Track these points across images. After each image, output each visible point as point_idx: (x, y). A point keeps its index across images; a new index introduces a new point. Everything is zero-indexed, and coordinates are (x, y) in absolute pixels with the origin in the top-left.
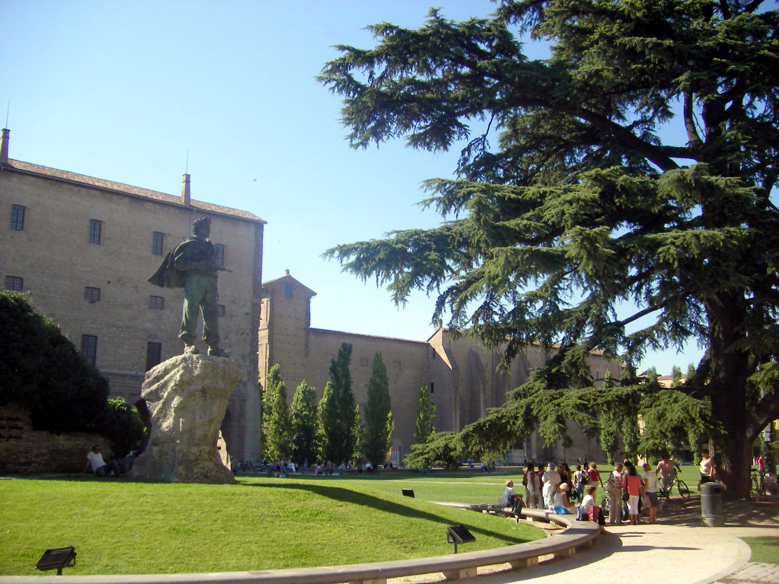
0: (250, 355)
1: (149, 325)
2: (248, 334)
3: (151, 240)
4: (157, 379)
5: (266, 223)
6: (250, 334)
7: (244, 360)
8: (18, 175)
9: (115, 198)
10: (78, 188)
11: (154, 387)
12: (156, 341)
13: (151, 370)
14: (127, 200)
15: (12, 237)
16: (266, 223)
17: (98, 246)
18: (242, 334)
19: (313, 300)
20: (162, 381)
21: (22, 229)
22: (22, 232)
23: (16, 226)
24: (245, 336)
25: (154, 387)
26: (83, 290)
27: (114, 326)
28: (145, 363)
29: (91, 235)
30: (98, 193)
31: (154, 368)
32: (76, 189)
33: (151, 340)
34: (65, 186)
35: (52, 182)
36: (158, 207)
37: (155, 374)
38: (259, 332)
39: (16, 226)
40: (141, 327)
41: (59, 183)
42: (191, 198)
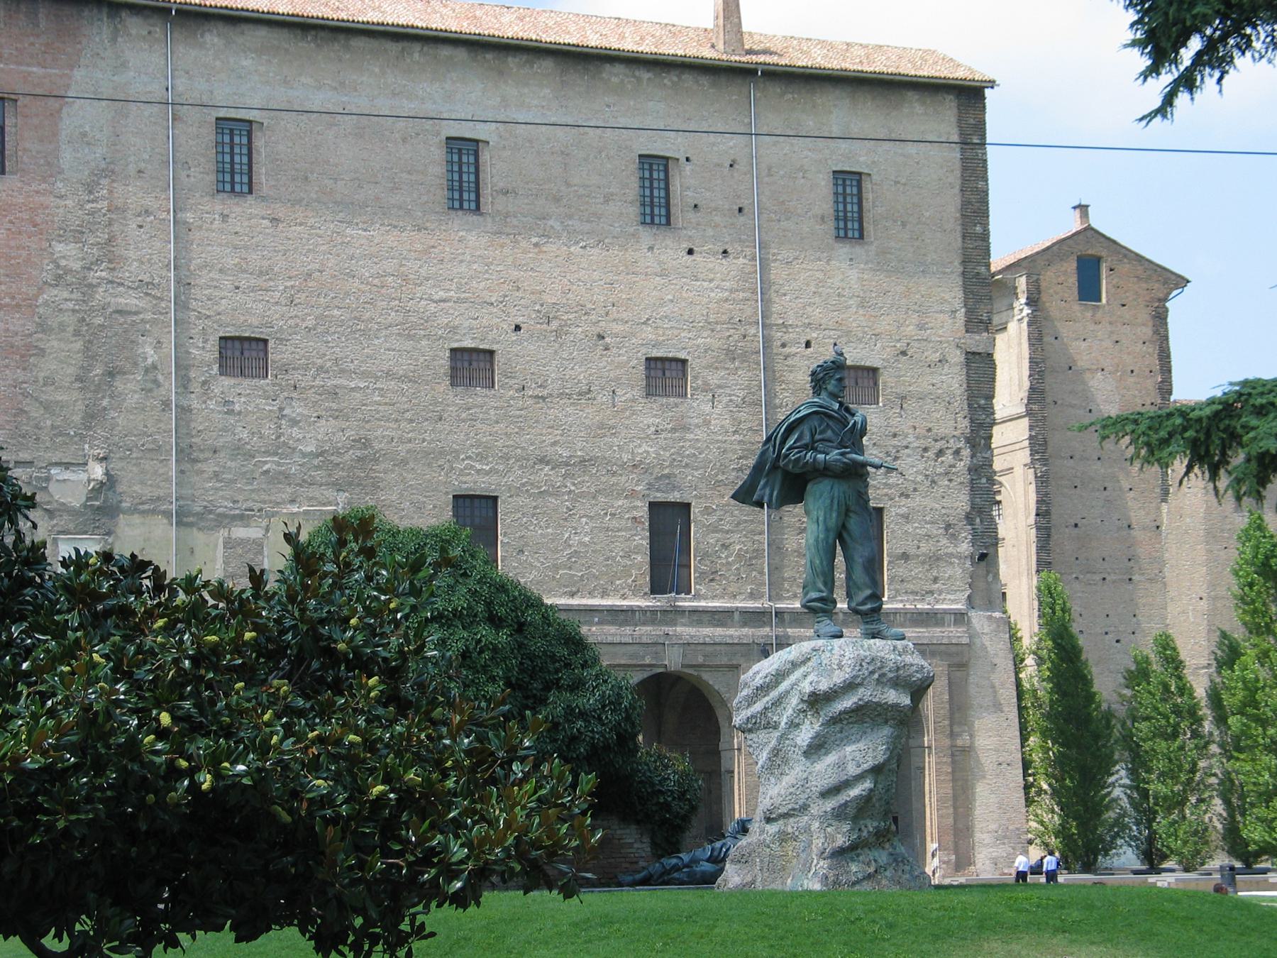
0: (969, 518)
1: (646, 450)
2: (957, 452)
3: (634, 183)
4: (763, 689)
5: (992, 84)
6: (966, 452)
7: (954, 537)
8: (220, 25)
9: (512, 61)
10: (400, 45)
11: (758, 707)
12: (674, 497)
13: (751, 673)
14: (548, 64)
15: (224, 217)
16: (992, 84)
17: (474, 218)
18: (941, 453)
19: (1176, 306)
20: (774, 694)
21: (250, 192)
22: (249, 197)
23: (233, 183)
24: (948, 458)
25: (758, 707)
26: (444, 360)
27: (543, 460)
28: (647, 567)
29: (451, 189)
30: (461, 54)
31: (756, 667)
32: (393, 47)
33: (660, 497)
34: (358, 43)
35: (322, 34)
36: (645, 75)
37: (758, 681)
38: (996, 430)
39: (233, 183)
40: (625, 457)
41: (342, 37)
42: (745, 29)
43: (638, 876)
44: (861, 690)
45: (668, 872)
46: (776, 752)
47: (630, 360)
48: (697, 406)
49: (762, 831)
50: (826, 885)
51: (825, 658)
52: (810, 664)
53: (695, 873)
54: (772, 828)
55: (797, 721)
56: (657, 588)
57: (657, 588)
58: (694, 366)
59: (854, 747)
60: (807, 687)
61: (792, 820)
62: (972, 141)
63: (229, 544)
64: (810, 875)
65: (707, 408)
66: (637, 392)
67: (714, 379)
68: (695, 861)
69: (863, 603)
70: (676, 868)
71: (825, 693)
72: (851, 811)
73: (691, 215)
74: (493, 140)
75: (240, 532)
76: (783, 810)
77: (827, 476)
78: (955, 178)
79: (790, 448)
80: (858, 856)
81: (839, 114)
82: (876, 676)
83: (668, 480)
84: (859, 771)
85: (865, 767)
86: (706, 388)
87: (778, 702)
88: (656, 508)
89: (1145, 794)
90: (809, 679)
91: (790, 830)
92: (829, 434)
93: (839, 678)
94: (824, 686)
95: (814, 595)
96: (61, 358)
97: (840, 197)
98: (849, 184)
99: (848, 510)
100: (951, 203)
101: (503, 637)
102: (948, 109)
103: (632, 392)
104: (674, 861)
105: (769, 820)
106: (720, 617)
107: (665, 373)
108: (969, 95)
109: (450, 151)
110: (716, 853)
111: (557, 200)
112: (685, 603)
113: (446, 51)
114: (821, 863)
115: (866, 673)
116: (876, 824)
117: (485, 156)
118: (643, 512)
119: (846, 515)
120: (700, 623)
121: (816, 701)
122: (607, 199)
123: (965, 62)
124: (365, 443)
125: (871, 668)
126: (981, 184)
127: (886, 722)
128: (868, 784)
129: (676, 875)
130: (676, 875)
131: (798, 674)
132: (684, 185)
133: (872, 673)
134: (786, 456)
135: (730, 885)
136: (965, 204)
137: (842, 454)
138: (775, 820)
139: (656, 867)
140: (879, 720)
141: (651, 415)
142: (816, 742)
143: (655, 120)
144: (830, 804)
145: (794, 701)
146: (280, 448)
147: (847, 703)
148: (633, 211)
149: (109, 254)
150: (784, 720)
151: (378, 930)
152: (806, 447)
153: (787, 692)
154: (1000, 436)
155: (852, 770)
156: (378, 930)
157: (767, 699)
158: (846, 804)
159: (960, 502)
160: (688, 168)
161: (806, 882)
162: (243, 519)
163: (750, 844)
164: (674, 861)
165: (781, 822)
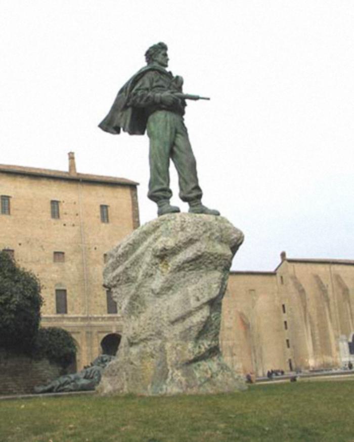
1: (55, 276)
11: (120, 269)
12: (62, 288)
20: (132, 258)
25: (120, 269)
43: (46, 388)
44: (198, 244)
45: (63, 385)
46: (135, 298)
47: (50, 252)
48: (68, 264)
49: (127, 353)
50: (182, 388)
51: (170, 225)
52: (159, 230)
53: (78, 385)
54: (134, 350)
55: (150, 272)
56: (58, 312)
57: (58, 312)
58: (66, 254)
59: (194, 287)
60: (159, 245)
61: (149, 343)
64: (168, 380)
65: (70, 265)
66: (52, 261)
67: (72, 257)
68: (77, 379)
69: (190, 193)
70: (67, 383)
71: (172, 248)
72: (194, 333)
73: (65, 216)
74: (13, 196)
76: (143, 336)
77: (161, 109)
79: (138, 90)
80: (199, 365)
81: (101, 191)
82: (208, 234)
83: (60, 284)
84: (198, 304)
85: (205, 300)
86: (70, 260)
87: (136, 262)
88: (57, 291)
90: (161, 239)
91: (148, 350)
92: (161, 83)
93: (182, 237)
94: (171, 243)
95: (157, 187)
97: (102, 212)
98: (104, 208)
99: (176, 132)
100: (130, 213)
101: (13, 316)
103: (50, 261)
104: (66, 379)
105: (131, 344)
106: (75, 319)
107: (59, 256)
109: (2, 199)
110: (89, 374)
111: (30, 211)
112: (65, 315)
114: (176, 372)
115: (201, 232)
116: (209, 343)
117: (11, 200)
118: (54, 292)
119: (176, 136)
120: (70, 321)
121: (163, 256)
122: (43, 212)
125: (204, 229)
126: (136, 209)
127: (216, 268)
128: (205, 312)
129: (67, 387)
130: (67, 387)
131: (150, 239)
132: (62, 209)
133: (205, 232)
134: (135, 94)
135: (105, 391)
136: (133, 214)
137: (172, 93)
138: (136, 344)
139: (57, 383)
140: (211, 267)
141: (55, 267)
142: (166, 285)
143: (55, 191)
144: (179, 328)
145: (148, 258)
147: (189, 253)
148: (50, 215)
150: (141, 273)
152: (147, 89)
153: (143, 254)
155: (194, 304)
157: (127, 262)
158: (190, 329)
160: (64, 204)
161: (164, 387)
163: (118, 363)
164: (66, 379)
165: (141, 345)
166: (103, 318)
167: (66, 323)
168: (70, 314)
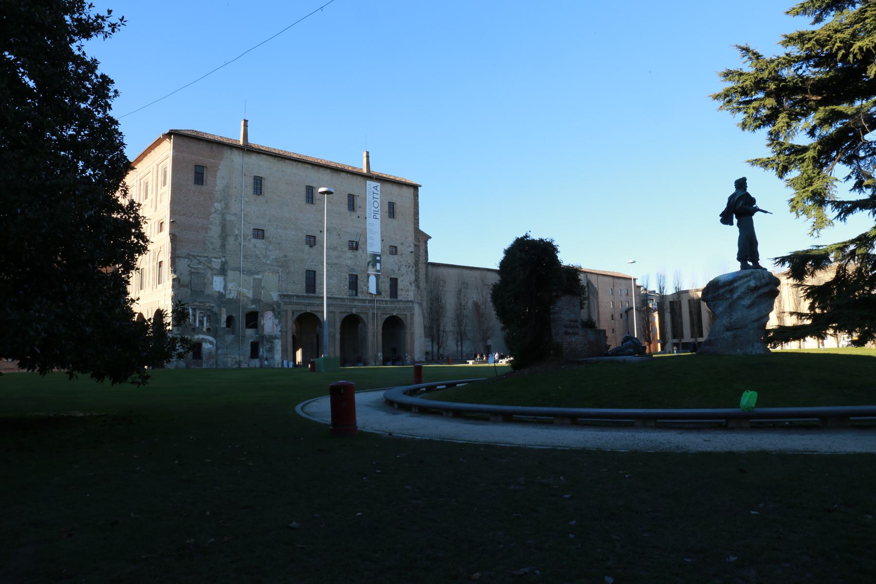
1: (349, 262)
14: (328, 171)
30: (310, 166)
32: (295, 163)
62: (416, 196)
63: (254, 279)
75: (256, 276)
78: (412, 206)
83: (353, 270)
89: (225, 220)
96: (215, 231)
100: (412, 212)
102: (412, 190)
108: (415, 187)
113: (307, 165)
120: (740, 429)
123: (414, 181)
124: (285, 256)
141: (350, 254)
146: (266, 256)
149: (227, 206)
151: (814, 98)
154: (420, 265)
156: (814, 98)
159: (413, 278)
162: (258, 273)
166: (386, 302)
167: (356, 303)
168: (360, 296)
